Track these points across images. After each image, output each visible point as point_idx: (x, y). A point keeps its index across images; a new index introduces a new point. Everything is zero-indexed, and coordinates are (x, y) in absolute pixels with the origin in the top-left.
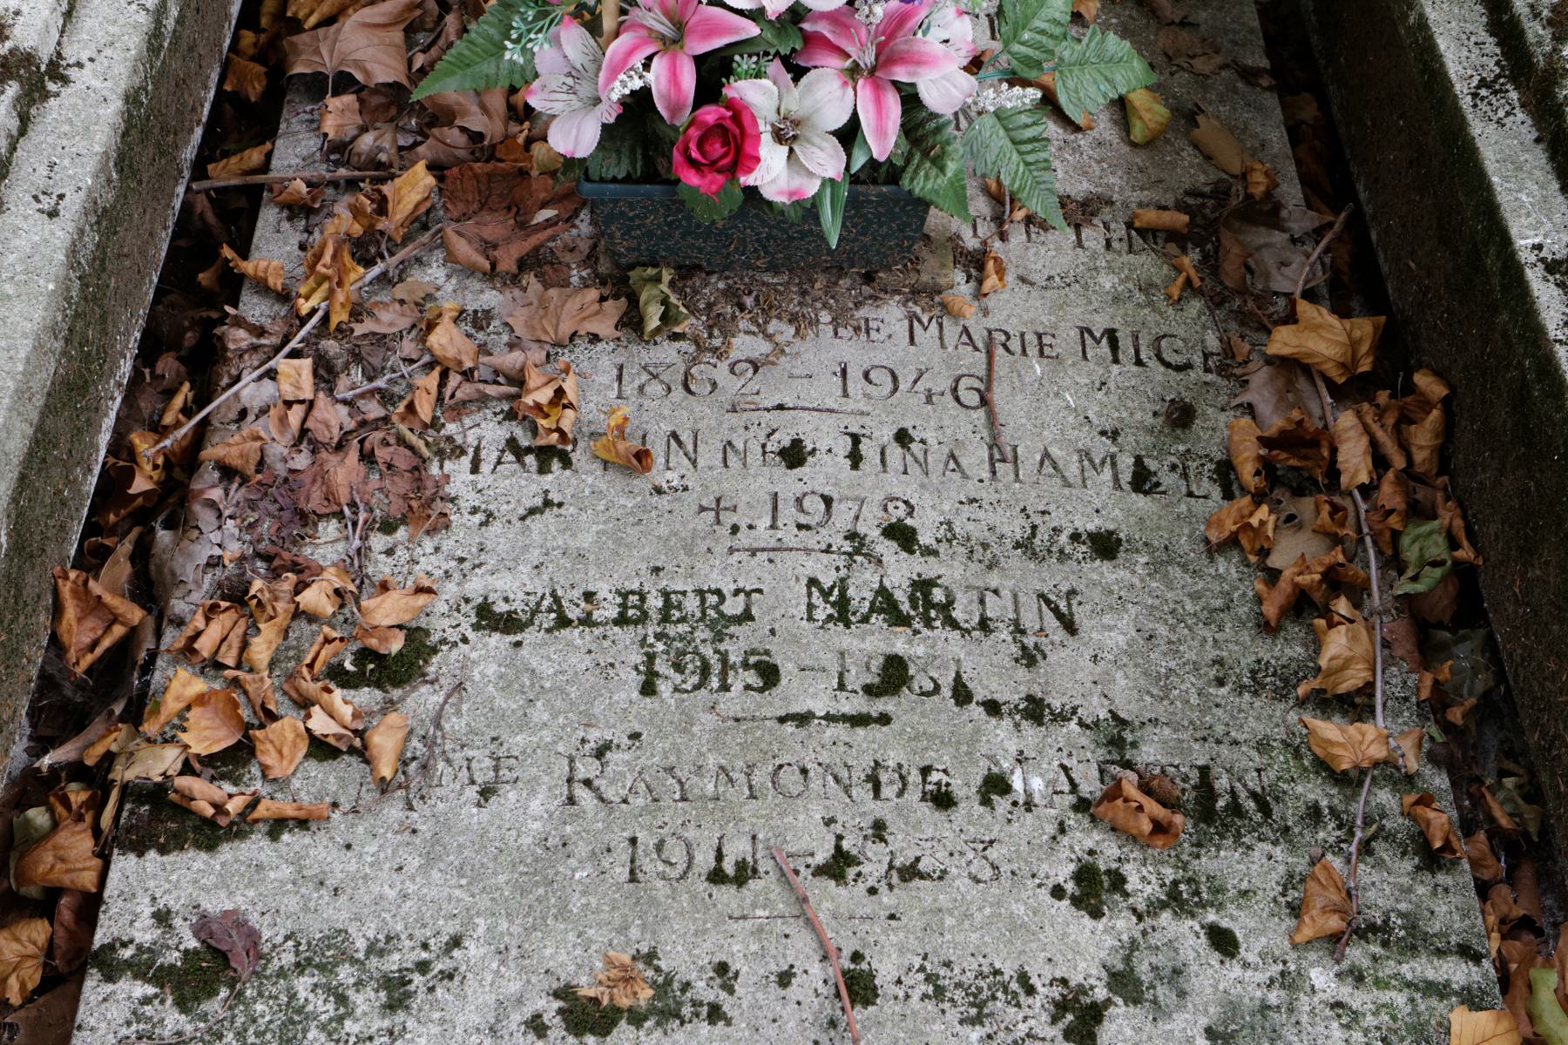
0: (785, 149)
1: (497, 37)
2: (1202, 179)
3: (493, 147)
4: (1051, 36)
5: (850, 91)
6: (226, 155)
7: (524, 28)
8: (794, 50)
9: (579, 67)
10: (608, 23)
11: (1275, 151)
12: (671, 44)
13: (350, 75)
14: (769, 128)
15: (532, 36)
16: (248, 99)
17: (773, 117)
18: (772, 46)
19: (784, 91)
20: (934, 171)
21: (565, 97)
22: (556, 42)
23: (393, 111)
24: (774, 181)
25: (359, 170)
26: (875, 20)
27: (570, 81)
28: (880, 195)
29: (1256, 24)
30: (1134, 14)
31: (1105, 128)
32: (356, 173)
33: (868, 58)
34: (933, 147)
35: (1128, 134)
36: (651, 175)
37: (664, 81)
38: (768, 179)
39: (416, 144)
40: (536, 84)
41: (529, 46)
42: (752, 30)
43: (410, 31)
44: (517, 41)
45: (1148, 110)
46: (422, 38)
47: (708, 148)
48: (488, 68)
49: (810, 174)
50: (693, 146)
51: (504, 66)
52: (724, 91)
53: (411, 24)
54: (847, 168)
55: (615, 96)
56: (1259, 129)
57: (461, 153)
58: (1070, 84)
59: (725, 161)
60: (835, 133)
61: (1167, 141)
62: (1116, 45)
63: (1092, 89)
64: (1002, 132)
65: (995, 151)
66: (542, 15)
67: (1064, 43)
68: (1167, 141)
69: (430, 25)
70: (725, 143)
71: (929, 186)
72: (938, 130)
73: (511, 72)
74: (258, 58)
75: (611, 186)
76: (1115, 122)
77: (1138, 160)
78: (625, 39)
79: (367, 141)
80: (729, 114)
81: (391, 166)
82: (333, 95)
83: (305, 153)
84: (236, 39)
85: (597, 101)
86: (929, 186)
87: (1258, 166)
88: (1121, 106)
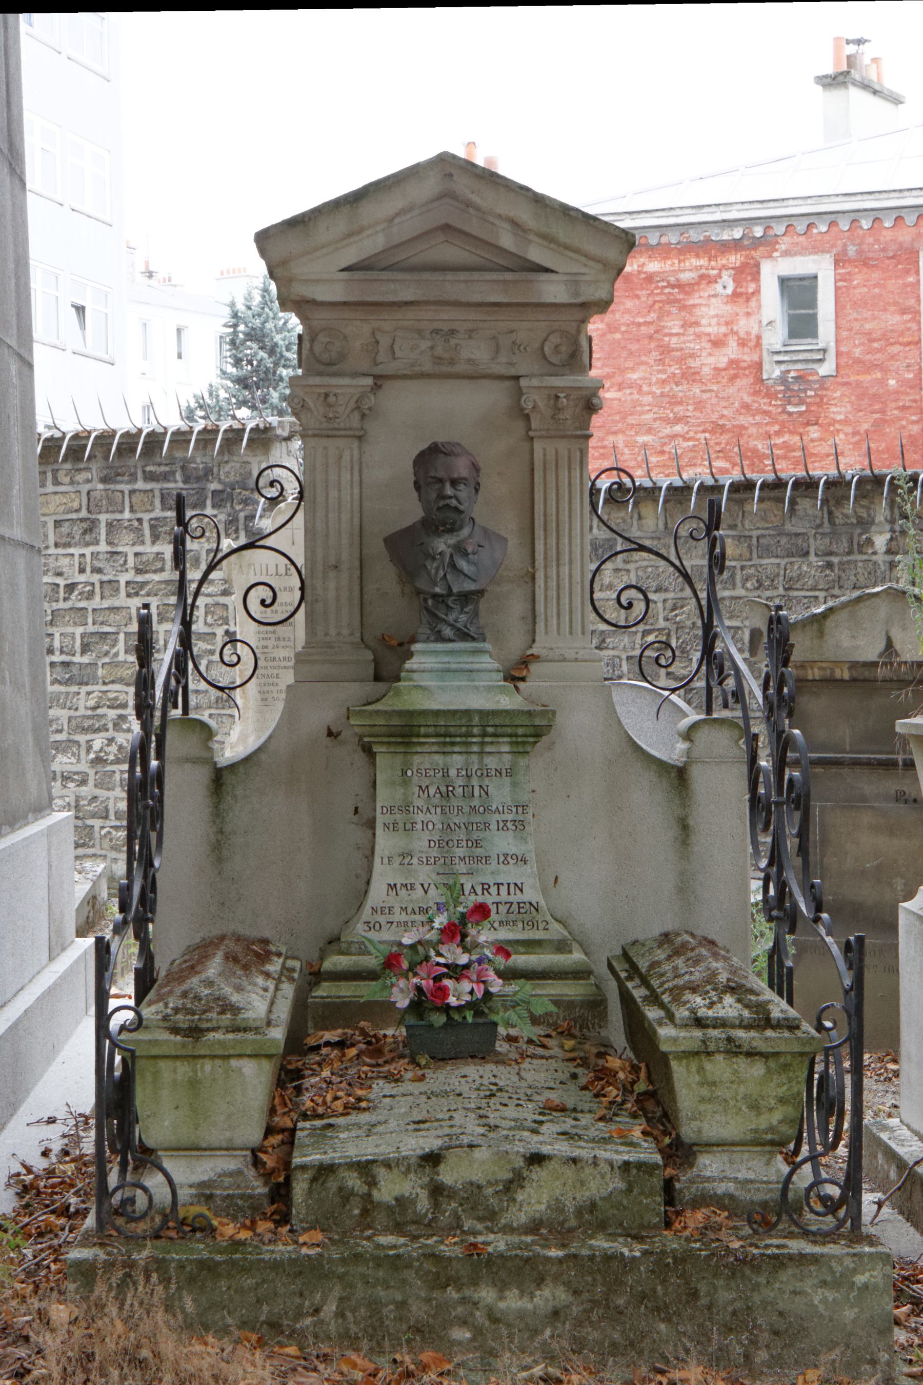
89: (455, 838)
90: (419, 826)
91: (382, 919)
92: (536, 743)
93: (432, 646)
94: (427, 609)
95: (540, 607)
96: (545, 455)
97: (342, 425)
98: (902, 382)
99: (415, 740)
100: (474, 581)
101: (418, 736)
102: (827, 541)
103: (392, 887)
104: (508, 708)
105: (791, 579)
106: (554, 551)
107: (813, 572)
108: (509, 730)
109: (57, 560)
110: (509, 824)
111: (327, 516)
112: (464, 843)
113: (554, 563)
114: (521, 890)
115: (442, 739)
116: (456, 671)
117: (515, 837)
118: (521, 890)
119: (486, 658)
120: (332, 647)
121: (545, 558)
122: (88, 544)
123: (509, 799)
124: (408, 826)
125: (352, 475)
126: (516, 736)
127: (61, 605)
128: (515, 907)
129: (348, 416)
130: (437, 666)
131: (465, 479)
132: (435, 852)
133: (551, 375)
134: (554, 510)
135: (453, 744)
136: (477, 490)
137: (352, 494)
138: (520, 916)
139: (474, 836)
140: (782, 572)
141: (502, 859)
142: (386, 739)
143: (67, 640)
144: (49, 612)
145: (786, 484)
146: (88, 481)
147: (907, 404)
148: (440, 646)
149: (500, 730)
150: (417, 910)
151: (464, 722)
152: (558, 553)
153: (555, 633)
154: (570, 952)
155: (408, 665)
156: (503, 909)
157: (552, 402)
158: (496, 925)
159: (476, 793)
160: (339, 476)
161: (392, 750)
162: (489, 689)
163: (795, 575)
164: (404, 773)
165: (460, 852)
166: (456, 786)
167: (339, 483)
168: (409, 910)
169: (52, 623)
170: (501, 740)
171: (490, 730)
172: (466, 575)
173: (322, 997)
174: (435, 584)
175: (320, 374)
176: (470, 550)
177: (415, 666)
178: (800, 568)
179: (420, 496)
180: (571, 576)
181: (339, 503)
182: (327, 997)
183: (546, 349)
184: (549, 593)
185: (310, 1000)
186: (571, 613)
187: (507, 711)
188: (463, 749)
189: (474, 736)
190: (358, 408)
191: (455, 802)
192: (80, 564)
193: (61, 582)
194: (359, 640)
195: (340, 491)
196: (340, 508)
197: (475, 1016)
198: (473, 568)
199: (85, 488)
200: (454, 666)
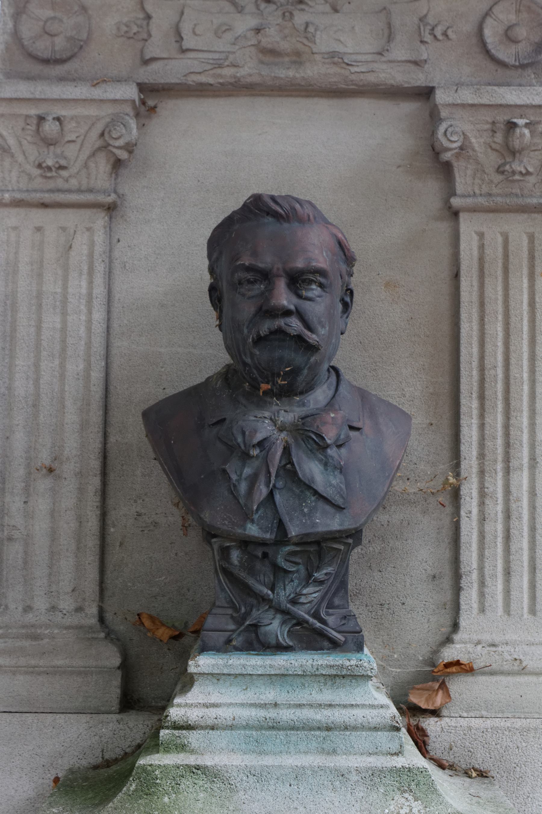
96: (482, 247)
97: (74, 183)
100: (339, 508)
106: (500, 441)
111: (37, 366)
113: (500, 466)
120: (36, 637)
121: (482, 456)
125: (91, 283)
129: (86, 166)
131: (322, 273)
133: (499, 85)
134: (500, 358)
136: (346, 307)
137: (89, 321)
152: (507, 445)
153: (500, 611)
157: (499, 138)
160: (65, 287)
167: (65, 301)
172: (316, 493)
174: (247, 517)
175: (30, 78)
176: (330, 436)
179: (220, 318)
181: (63, 341)
183: (488, 33)
184: (488, 527)
190: (105, 147)
194: (94, 621)
195: (64, 314)
196: (64, 349)
197: (302, 520)
198: (336, 480)
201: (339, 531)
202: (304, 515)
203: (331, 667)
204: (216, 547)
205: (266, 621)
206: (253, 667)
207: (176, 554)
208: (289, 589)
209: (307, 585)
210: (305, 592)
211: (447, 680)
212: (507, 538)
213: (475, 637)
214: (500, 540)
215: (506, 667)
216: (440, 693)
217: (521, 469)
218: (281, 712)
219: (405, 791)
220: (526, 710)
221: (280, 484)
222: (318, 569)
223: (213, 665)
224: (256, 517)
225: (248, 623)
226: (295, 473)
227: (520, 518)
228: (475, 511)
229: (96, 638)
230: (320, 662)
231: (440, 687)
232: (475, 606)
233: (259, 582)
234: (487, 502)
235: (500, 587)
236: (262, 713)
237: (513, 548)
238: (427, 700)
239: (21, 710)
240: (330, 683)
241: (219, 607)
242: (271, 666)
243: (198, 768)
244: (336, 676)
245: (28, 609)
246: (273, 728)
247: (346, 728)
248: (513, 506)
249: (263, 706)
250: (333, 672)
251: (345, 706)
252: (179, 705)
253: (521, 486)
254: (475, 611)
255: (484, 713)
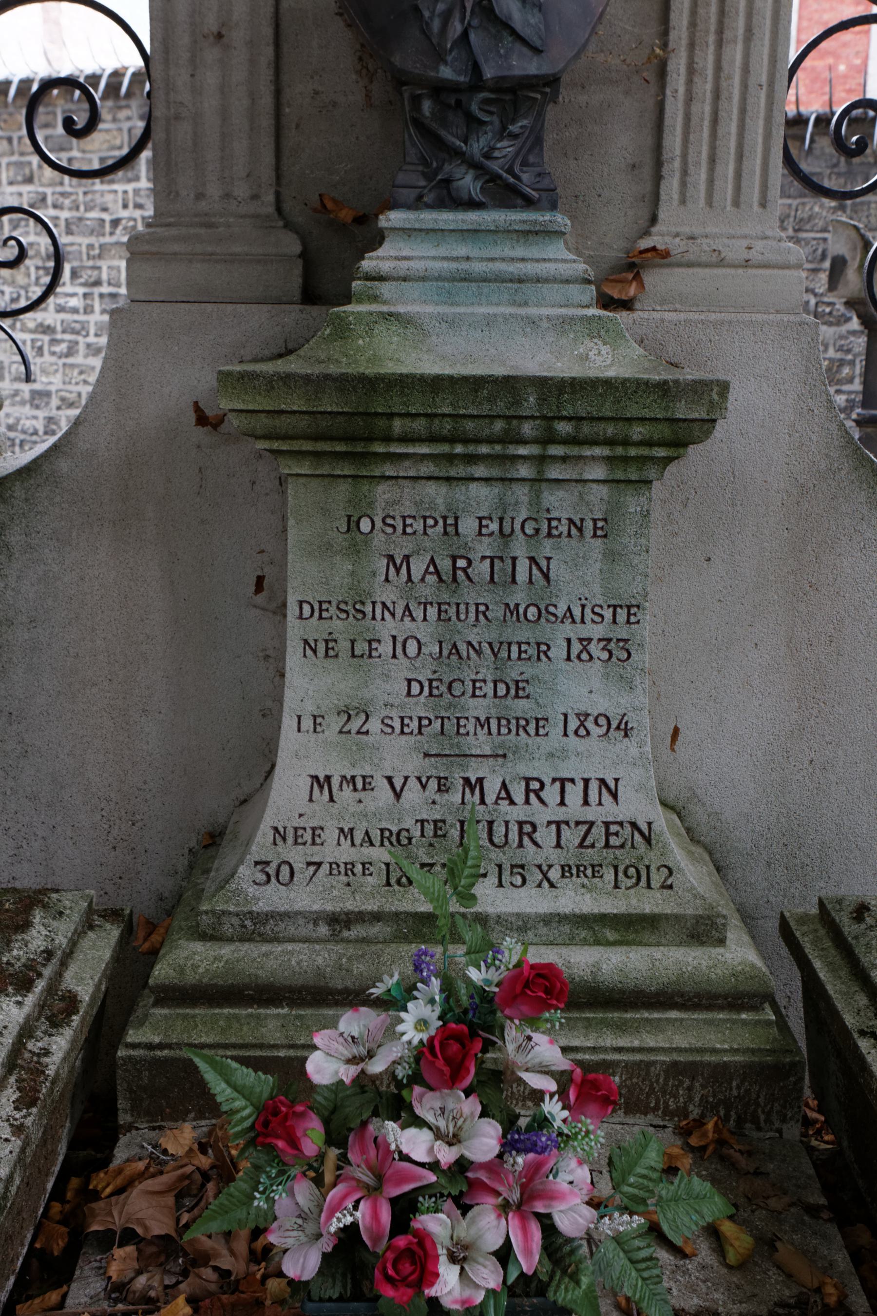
0: (456, 1269)
1: (249, 1190)
2: (787, 1293)
3: (237, 1281)
4: (650, 1180)
5: (504, 1221)
6: (30, 1298)
7: (268, 1183)
8: (461, 1192)
9: (306, 1210)
10: (328, 1178)
11: (841, 1269)
12: (372, 1191)
13: (133, 1230)
14: (445, 1251)
15: (275, 1188)
16: (52, 1253)
17: (447, 1242)
18: (446, 1188)
19: (455, 1222)
20: (572, 1285)
21: (295, 1233)
22: (291, 1193)
23: (162, 1258)
24: (450, 1292)
25: (133, 1304)
26: (519, 1168)
27: (300, 1221)
28: (532, 1305)
29: (812, 1172)
30: (719, 1167)
31: (705, 1253)
32: (131, 1307)
33: (515, 1196)
34: (570, 1265)
35: (724, 1258)
36: (358, 1296)
37: (368, 1218)
38: (445, 1291)
39: (178, 1283)
40: (275, 1225)
41: (272, 1195)
42: (432, 1178)
43: (179, 1197)
44: (263, 1193)
45: (737, 1239)
46: (188, 1202)
47: (401, 1267)
48: (241, 1214)
49: (477, 1286)
50: (389, 1266)
51: (253, 1211)
52: (412, 1224)
53: (180, 1192)
54: (504, 1282)
55: (333, 1229)
56: (826, 1252)
57: (213, 1287)
58: (670, 1215)
59: (413, 1277)
60: (495, 1254)
61: (756, 1264)
62: (700, 1185)
63: (686, 1219)
64: (622, 1254)
65: (618, 1268)
66: (281, 1173)
67: (661, 1185)
68: (756, 1264)
69: (195, 1192)
70: (413, 1263)
71: (569, 1297)
72: (572, 1252)
73: (257, 1216)
74: (63, 1222)
75: (328, 1304)
76: (714, 1250)
77: (735, 1279)
78: (340, 1188)
79: (142, 1280)
80: (416, 1240)
81: (158, 1301)
82: (119, 1247)
83: (92, 1293)
84: (47, 1208)
85: (319, 1236)
86: (569, 1297)
87: (828, 1280)
88: (713, 1232)
89: (469, 675)
90: (386, 648)
91: (297, 856)
92: (669, 460)
93: (429, 218)
94: (418, 124)
95: (673, 142)
98: (851, 67)
99: (379, 448)
100: (537, 51)
101: (388, 439)
102: (842, 181)
103: (321, 782)
104: (611, 373)
105: (801, 220)
107: (824, 214)
108: (610, 430)
109: (102, 196)
110: (594, 648)
112: (489, 689)
113: (712, 38)
114: (615, 796)
115: (445, 448)
116: (484, 279)
117: (606, 676)
118: (615, 796)
119: (557, 250)
120: (210, 226)
121: (693, 25)
122: (129, 181)
123: (597, 588)
124: (361, 647)
126: (626, 443)
127: (107, 239)
128: (598, 832)
130: (438, 265)
132: (420, 707)
135: (471, 459)
138: (609, 854)
139: (513, 673)
140: (793, 213)
141: (573, 724)
142: (307, 446)
143: (114, 273)
144: (97, 245)
145: (807, 121)
146: (129, 118)
147: (853, 87)
148: (447, 218)
149: (586, 429)
150: (376, 835)
151: (500, 407)
153: (702, 202)
154: (721, 942)
155: (367, 264)
156: (571, 836)
158: (554, 874)
159: (522, 575)
161: (325, 470)
162: (564, 324)
163: (806, 216)
164: (352, 524)
165: (478, 708)
166: (475, 557)
168: (359, 836)
169: (100, 256)
170: (587, 452)
171: (564, 428)
172: (513, 32)
173: (150, 1047)
174: (439, 56)
177: (386, 267)
178: (811, 209)
180: (746, 70)
182: (161, 1046)
184: (695, 109)
185: (121, 1053)
186: (740, 156)
187: (608, 383)
188: (495, 472)
189: (523, 442)
191: (470, 595)
192: (124, 200)
193: (107, 217)
194: (271, 209)
198: (534, 18)
199: (126, 126)
200: (478, 267)
201: (536, 76)
202: (501, 56)
203: (524, 222)
204: (406, 95)
205: (458, 176)
206: (446, 221)
207: (357, 138)
208: (483, 141)
209: (501, 139)
210: (499, 145)
211: (641, 271)
212: (715, 120)
213: (673, 229)
214: (706, 123)
215: (704, 258)
216: (634, 285)
217: (735, 42)
218: (473, 265)
219: (594, 337)
220: (721, 304)
221: (475, 22)
222: (513, 121)
223: (404, 220)
224: (449, 58)
225: (439, 177)
226: (492, 10)
227: (730, 99)
228: (682, 90)
229: (274, 227)
230: (513, 218)
231: (634, 278)
232: (676, 197)
233: (452, 134)
234: (696, 79)
235: (703, 176)
236: (454, 265)
237: (721, 132)
238: (620, 292)
239: (200, 299)
240: (522, 240)
241: (409, 164)
242: (463, 221)
243: (391, 314)
244: (529, 232)
245: (200, 196)
246: (465, 280)
247: (538, 281)
248: (724, 84)
249: (456, 259)
250: (526, 227)
251: (538, 261)
252: (371, 258)
253: (733, 62)
254: (675, 203)
255: (678, 306)
